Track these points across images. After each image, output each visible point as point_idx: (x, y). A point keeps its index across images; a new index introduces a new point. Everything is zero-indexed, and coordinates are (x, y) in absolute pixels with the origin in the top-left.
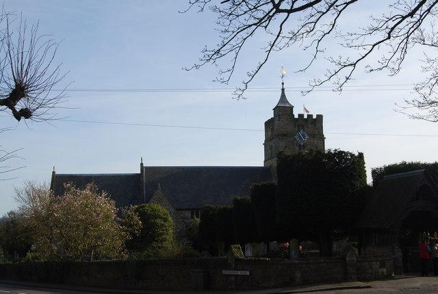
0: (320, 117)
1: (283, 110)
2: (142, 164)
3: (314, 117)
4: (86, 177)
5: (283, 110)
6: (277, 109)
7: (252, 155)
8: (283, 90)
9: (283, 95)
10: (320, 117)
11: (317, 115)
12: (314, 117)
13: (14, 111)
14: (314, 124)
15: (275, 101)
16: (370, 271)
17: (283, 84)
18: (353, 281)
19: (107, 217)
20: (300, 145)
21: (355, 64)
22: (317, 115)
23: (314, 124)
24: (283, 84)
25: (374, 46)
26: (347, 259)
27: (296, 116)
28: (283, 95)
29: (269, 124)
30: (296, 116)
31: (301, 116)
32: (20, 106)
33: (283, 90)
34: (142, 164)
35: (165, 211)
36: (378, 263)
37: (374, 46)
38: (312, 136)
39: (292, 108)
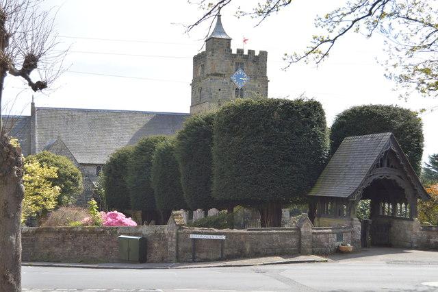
0: (264, 54)
1: (218, 44)
2: (33, 104)
3: (257, 54)
5: (218, 44)
6: (210, 41)
7: (178, 100)
10: (264, 54)
11: (261, 52)
12: (257, 54)
13: (31, 84)
14: (257, 62)
15: (206, 29)
16: (326, 244)
18: (307, 254)
19: (432, 184)
20: (237, 89)
21: (333, 41)
22: (261, 52)
23: (257, 62)
25: (354, 22)
26: (302, 230)
27: (234, 52)
30: (234, 52)
31: (240, 51)
32: (35, 76)
34: (33, 104)
36: (335, 235)
37: (354, 22)
38: (254, 77)
39: (229, 40)
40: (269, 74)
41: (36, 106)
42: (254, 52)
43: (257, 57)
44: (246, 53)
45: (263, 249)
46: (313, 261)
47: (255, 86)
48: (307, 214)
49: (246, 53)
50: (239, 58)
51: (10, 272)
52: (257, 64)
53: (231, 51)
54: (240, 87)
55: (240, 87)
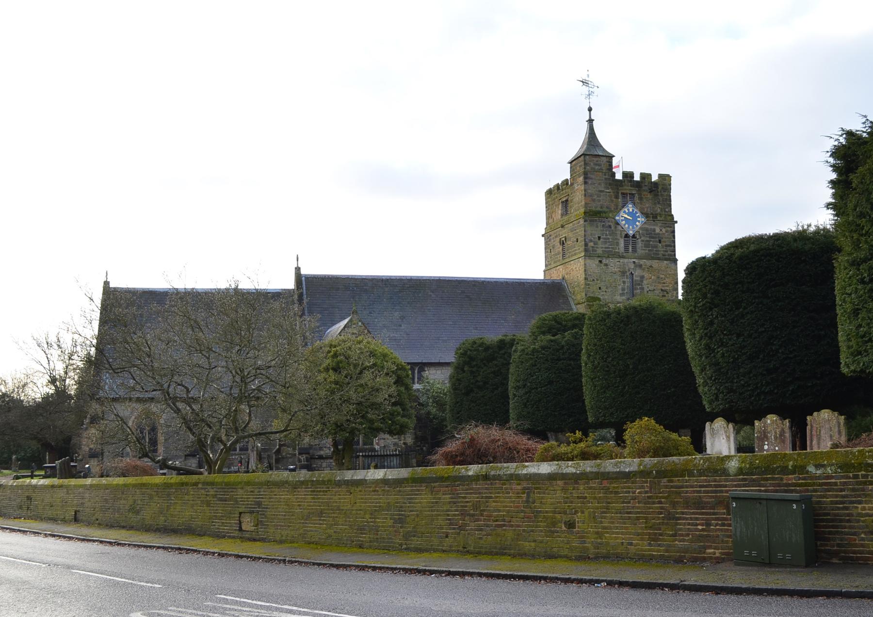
0: (665, 179)
2: (298, 269)
4: (483, 282)
8: (591, 121)
9: (592, 138)
10: (665, 179)
11: (660, 176)
12: (655, 178)
15: (575, 145)
17: (590, 109)
20: (627, 236)
22: (660, 176)
24: (590, 109)
27: (619, 176)
28: (592, 138)
29: (693, 261)
30: (619, 176)
33: (591, 121)
34: (298, 269)
35: (537, 317)
38: (652, 217)
40: (675, 211)
41: (112, 285)
42: (650, 175)
43: (655, 184)
44: (637, 178)
45: (65, 588)
46: (463, 574)
47: (654, 230)
48: (823, 438)
49: (637, 178)
50: (627, 189)
51: (768, 445)
52: (657, 195)
53: (614, 174)
54: (631, 233)
55: (631, 233)
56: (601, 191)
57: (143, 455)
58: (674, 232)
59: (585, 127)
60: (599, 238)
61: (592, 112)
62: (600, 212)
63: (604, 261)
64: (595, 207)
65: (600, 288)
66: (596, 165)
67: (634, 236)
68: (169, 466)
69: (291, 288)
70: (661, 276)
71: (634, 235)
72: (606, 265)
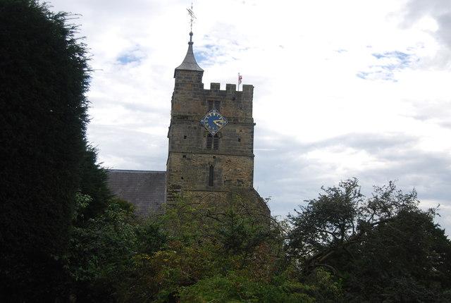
0: (249, 89)
8: (191, 44)
15: (178, 60)
17: (191, 34)
20: (210, 135)
24: (191, 34)
27: (207, 87)
30: (207, 87)
33: (191, 44)
44: (223, 88)
55: (213, 133)
56: (190, 99)
57: (389, 195)
58: (253, 132)
59: (187, 46)
60: (185, 137)
61: (193, 37)
62: (187, 117)
63: (188, 156)
64: (183, 111)
65: (182, 178)
66: (187, 78)
67: (216, 136)
68: (322, 222)
69: (94, 136)
70: (238, 169)
71: (216, 135)
72: (189, 159)
